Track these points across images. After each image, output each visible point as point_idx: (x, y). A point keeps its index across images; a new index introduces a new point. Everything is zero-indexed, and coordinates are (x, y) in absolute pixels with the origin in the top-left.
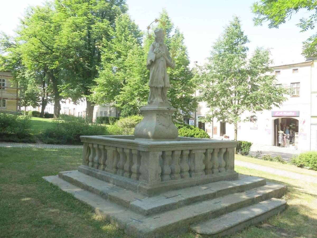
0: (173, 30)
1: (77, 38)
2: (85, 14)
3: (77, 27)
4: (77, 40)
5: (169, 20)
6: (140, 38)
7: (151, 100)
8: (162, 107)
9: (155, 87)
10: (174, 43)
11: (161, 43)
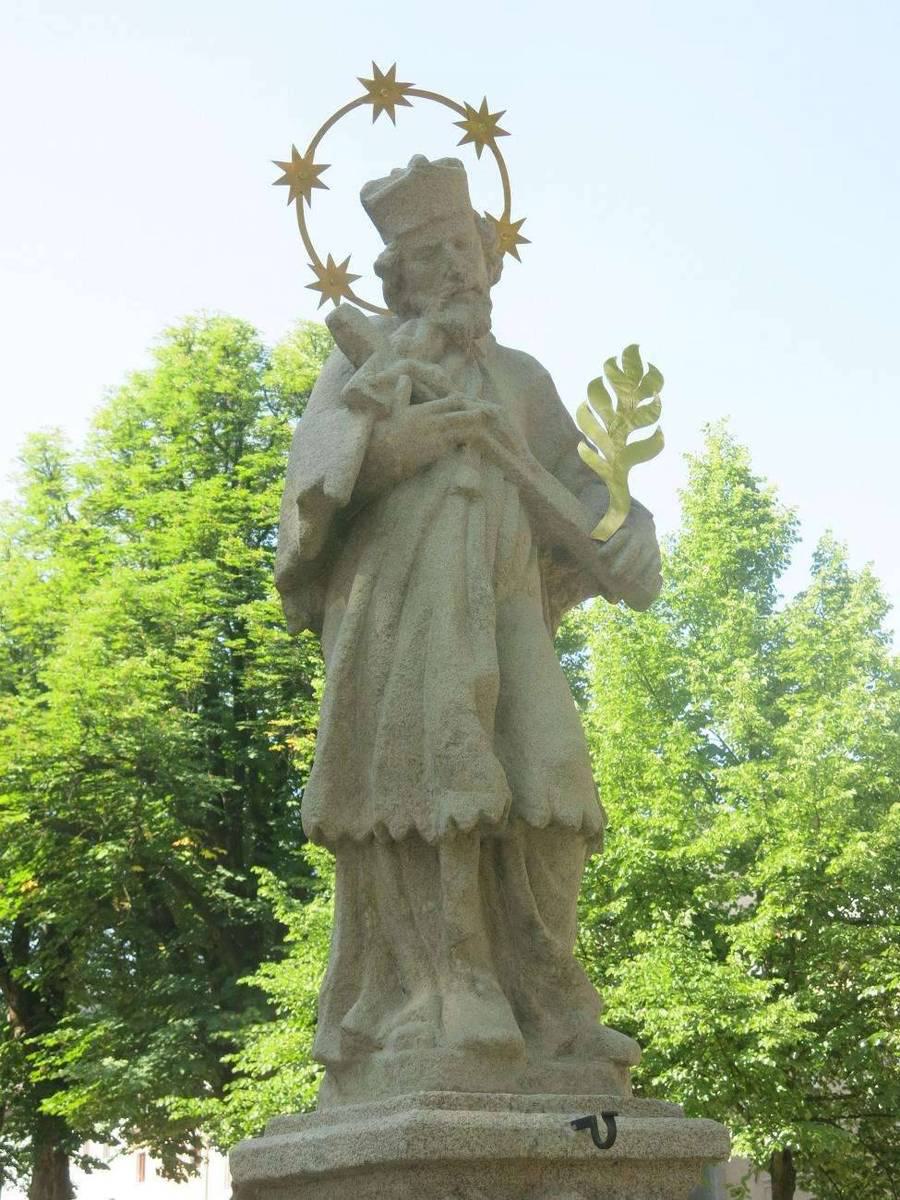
0: (800, 557)
1: (144, 694)
2: (207, 547)
3: (150, 626)
4: (138, 708)
5: (760, 496)
6: (575, 658)
7: (349, 1020)
8: (484, 1118)
9: (392, 844)
10: (812, 642)
11: (459, 315)
